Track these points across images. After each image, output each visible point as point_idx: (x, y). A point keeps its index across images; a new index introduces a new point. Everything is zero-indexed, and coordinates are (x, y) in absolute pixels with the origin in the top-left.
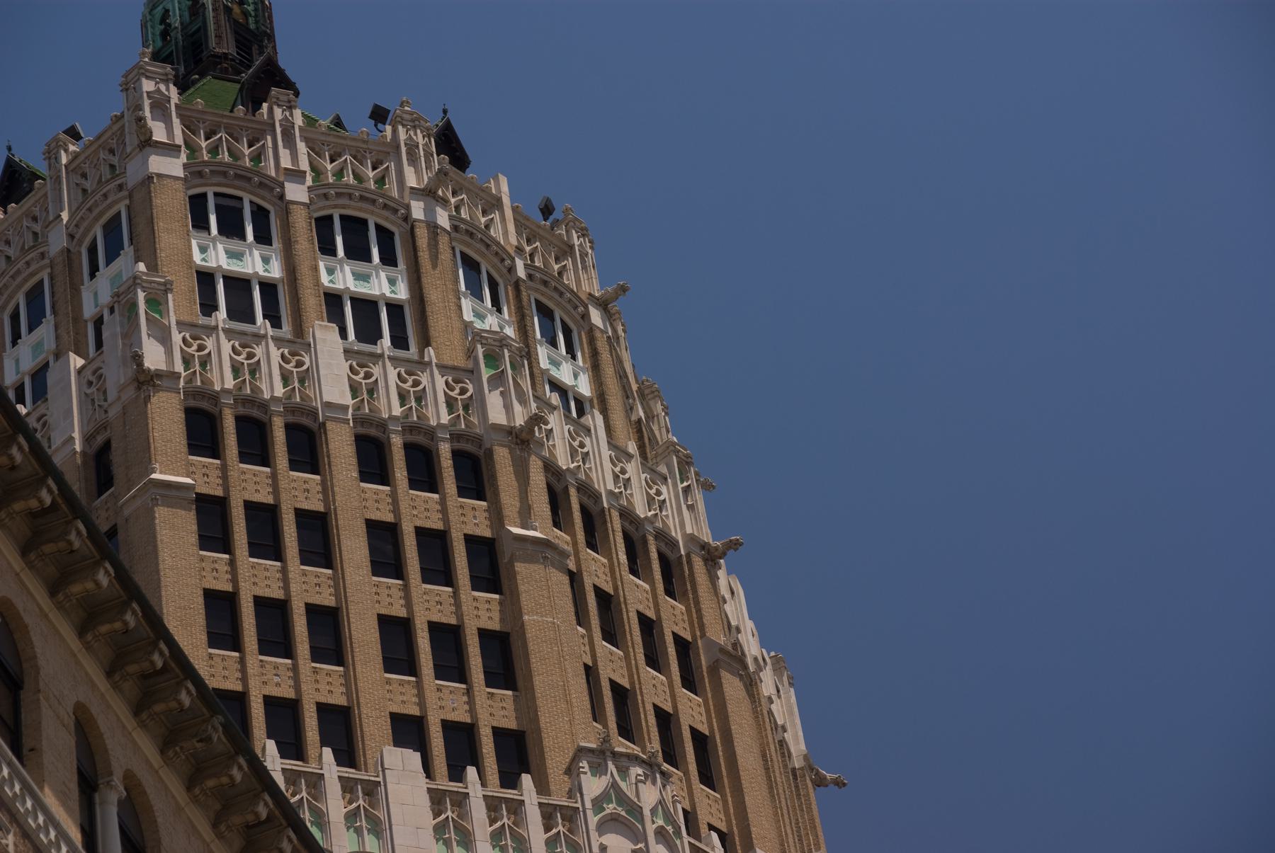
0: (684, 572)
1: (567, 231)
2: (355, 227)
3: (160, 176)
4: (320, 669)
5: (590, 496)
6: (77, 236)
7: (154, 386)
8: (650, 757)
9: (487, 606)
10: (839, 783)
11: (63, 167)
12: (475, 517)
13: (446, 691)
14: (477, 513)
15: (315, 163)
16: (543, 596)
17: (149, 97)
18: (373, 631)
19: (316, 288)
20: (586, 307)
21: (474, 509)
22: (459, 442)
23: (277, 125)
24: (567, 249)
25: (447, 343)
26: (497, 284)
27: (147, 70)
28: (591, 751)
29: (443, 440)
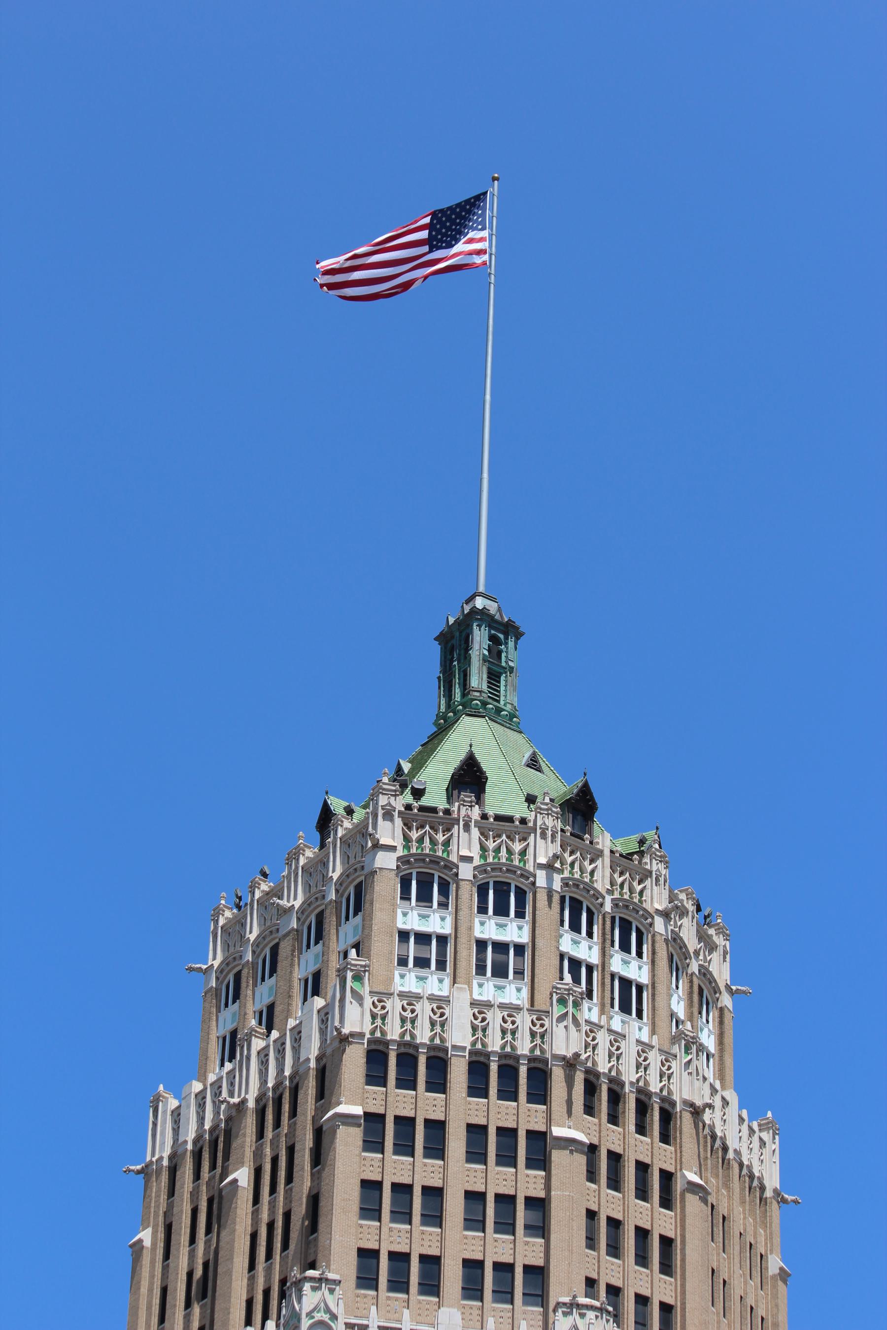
0: (676, 1124)
1: (650, 860)
2: (502, 890)
3: (380, 869)
4: (426, 1231)
5: (618, 1084)
6: (340, 892)
7: (349, 1041)
8: (602, 1304)
9: (534, 1180)
10: (796, 1202)
11: (339, 839)
12: (536, 1117)
13: (500, 1242)
14: (538, 1114)
15: (483, 844)
16: (566, 1177)
17: (383, 809)
18: (460, 1205)
19: (469, 943)
20: (653, 918)
21: (536, 1111)
22: (534, 1063)
23: (461, 820)
24: (648, 874)
25: (545, 978)
26: (593, 914)
27: (384, 789)
28: (565, 1304)
29: (523, 1064)
